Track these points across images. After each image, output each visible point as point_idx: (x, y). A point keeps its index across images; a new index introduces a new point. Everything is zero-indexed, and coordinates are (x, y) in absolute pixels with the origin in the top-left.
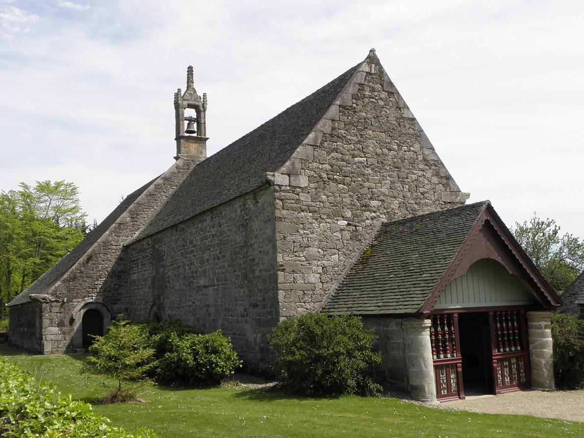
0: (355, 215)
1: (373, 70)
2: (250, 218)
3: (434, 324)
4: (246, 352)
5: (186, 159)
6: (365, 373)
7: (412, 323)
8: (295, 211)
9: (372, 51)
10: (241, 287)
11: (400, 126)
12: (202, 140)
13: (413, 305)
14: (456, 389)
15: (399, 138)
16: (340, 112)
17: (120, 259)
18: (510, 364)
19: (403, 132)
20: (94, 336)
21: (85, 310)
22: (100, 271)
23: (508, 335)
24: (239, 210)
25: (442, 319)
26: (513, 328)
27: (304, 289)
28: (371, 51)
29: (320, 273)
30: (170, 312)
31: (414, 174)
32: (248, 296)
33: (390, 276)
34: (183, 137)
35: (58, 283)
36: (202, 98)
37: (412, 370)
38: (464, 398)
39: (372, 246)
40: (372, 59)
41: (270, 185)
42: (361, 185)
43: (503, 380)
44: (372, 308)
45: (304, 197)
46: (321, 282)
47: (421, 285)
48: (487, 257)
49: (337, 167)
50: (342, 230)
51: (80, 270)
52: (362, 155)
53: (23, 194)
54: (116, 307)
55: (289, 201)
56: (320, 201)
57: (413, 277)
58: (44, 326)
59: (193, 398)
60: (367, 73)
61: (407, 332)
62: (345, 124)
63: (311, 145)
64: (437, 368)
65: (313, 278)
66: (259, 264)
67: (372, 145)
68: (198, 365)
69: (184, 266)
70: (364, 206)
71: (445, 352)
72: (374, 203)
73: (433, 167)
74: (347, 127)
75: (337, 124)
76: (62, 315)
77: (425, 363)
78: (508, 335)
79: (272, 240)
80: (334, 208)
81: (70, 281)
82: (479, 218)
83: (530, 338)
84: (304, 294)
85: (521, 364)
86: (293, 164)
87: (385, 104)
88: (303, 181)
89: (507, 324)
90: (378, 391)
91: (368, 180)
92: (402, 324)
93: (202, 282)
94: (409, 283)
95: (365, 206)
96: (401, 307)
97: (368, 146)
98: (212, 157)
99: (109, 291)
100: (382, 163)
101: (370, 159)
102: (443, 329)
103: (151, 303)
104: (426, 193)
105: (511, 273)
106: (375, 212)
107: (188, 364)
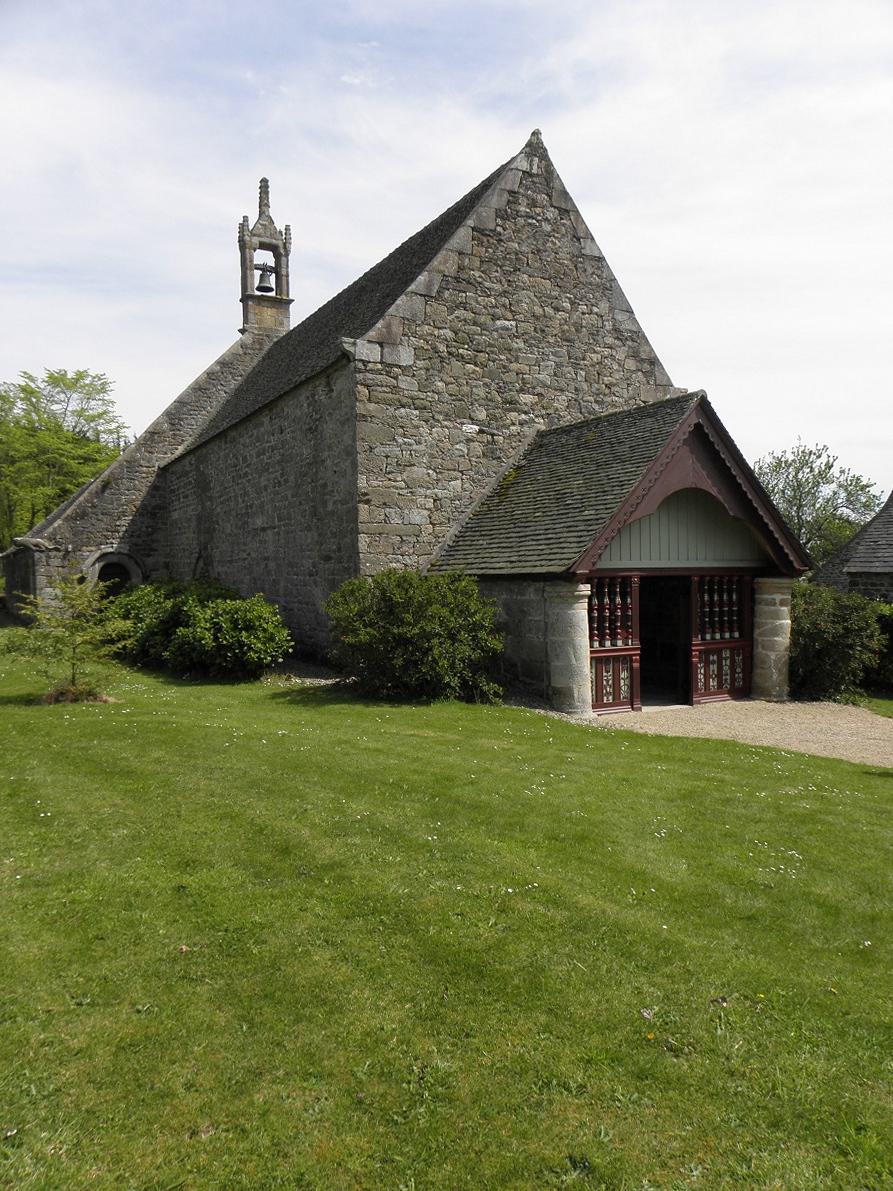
0: (492, 417)
1: (535, 167)
2: (321, 417)
3: (598, 592)
4: (315, 629)
5: (256, 332)
6: (474, 666)
7: (558, 589)
8: (390, 405)
9: (536, 134)
10: (308, 529)
11: (577, 269)
12: (282, 303)
13: (561, 559)
14: (629, 696)
15: (574, 291)
16: (473, 240)
17: (154, 488)
18: (720, 659)
19: (581, 279)
20: (24, 595)
21: (102, 564)
22: (123, 505)
23: (721, 613)
24: (305, 405)
25: (612, 586)
26: (731, 603)
27: (402, 533)
28: (533, 134)
29: (429, 509)
30: (220, 569)
31: (595, 352)
32: (317, 542)
33: (537, 514)
34: (253, 297)
35: (59, 522)
36: (284, 232)
37: (556, 663)
38: (640, 709)
39: (519, 468)
40: (535, 148)
41: (349, 361)
42: (504, 367)
43: (706, 684)
44: (501, 566)
45: (405, 383)
46: (431, 523)
47: (578, 529)
48: (694, 486)
49: (465, 335)
50: (469, 440)
51: (92, 503)
52: (509, 315)
53: (24, 389)
54: (150, 561)
55: (379, 389)
56: (433, 391)
57: (570, 515)
58: (38, 586)
59: (199, 698)
60: (524, 172)
61: (551, 603)
62: (482, 262)
63: (421, 295)
64: (598, 662)
65: (418, 517)
66: (333, 491)
67: (527, 300)
68: (220, 647)
69: (236, 496)
70: (508, 403)
71: (613, 637)
72: (526, 399)
73: (629, 343)
74: (485, 267)
75: (467, 260)
76: (66, 570)
77: (575, 653)
78: (721, 613)
79: (351, 453)
80: (458, 403)
81: (76, 520)
82: (686, 420)
83: (757, 620)
84: (403, 541)
85: (739, 659)
86: (388, 326)
87: (554, 230)
88: (406, 356)
89: (721, 596)
90: (496, 694)
91: (517, 360)
92: (544, 591)
93: (259, 522)
94: (562, 525)
95: (510, 403)
96: (543, 563)
97: (519, 302)
98: (295, 328)
99: (139, 536)
100: (543, 331)
102: (612, 600)
103: (197, 555)
104: (614, 385)
105: (731, 514)
106: (526, 413)
107: (204, 645)
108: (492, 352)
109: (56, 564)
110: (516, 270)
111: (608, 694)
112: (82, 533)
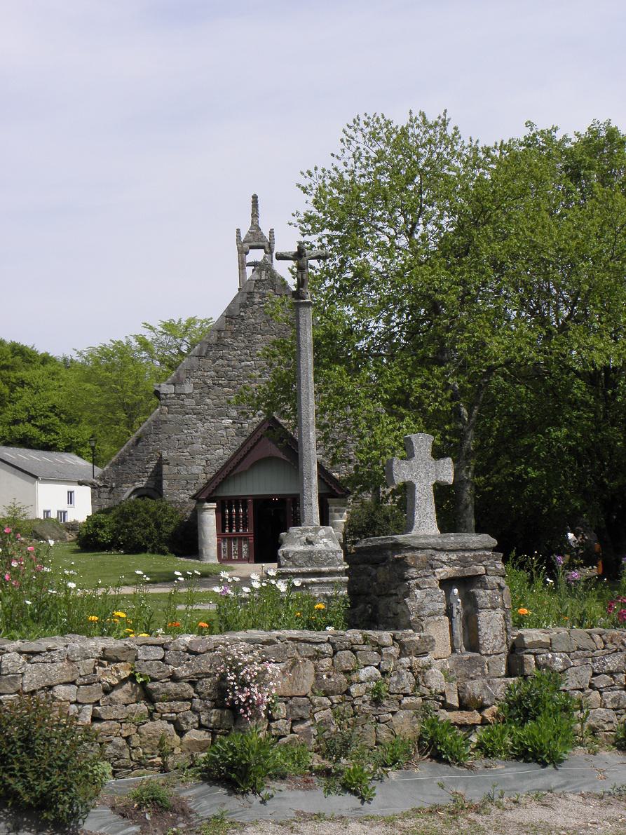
45: (188, 402)
50: (226, 428)
51: (129, 453)
55: (174, 407)
60: (256, 281)
84: (188, 483)
101: (258, 362)
108: (240, 380)
110: (253, 333)
111: (235, 555)
112: (122, 474)
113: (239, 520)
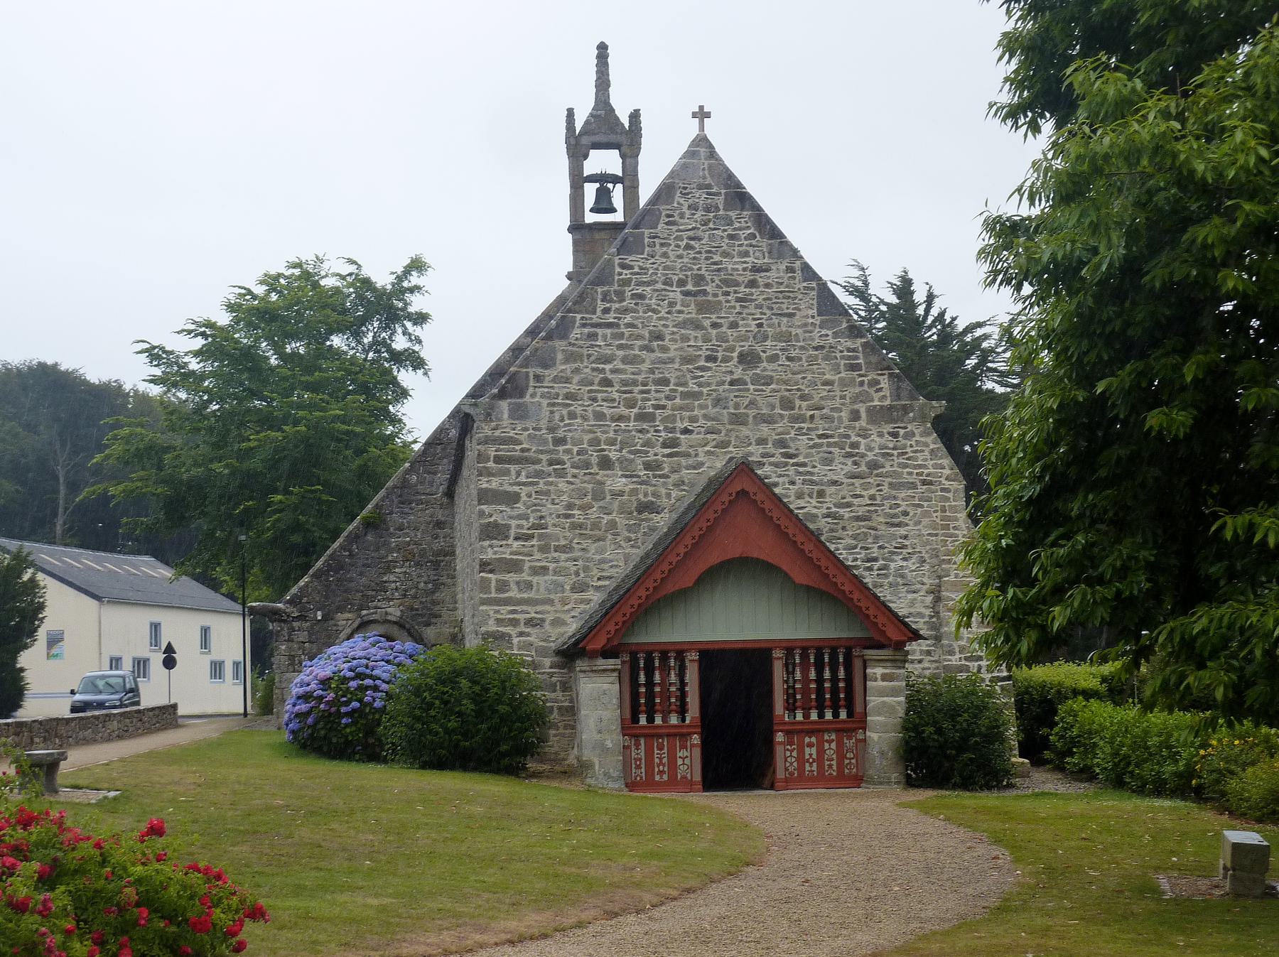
25: (664, 656)
99: (415, 597)
109: (301, 639)
113: (838, 693)
